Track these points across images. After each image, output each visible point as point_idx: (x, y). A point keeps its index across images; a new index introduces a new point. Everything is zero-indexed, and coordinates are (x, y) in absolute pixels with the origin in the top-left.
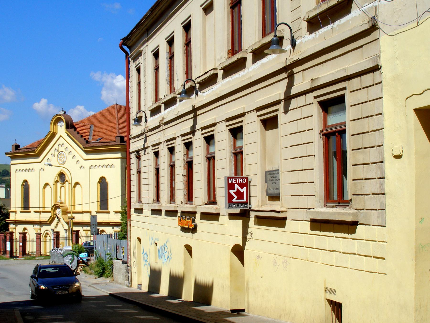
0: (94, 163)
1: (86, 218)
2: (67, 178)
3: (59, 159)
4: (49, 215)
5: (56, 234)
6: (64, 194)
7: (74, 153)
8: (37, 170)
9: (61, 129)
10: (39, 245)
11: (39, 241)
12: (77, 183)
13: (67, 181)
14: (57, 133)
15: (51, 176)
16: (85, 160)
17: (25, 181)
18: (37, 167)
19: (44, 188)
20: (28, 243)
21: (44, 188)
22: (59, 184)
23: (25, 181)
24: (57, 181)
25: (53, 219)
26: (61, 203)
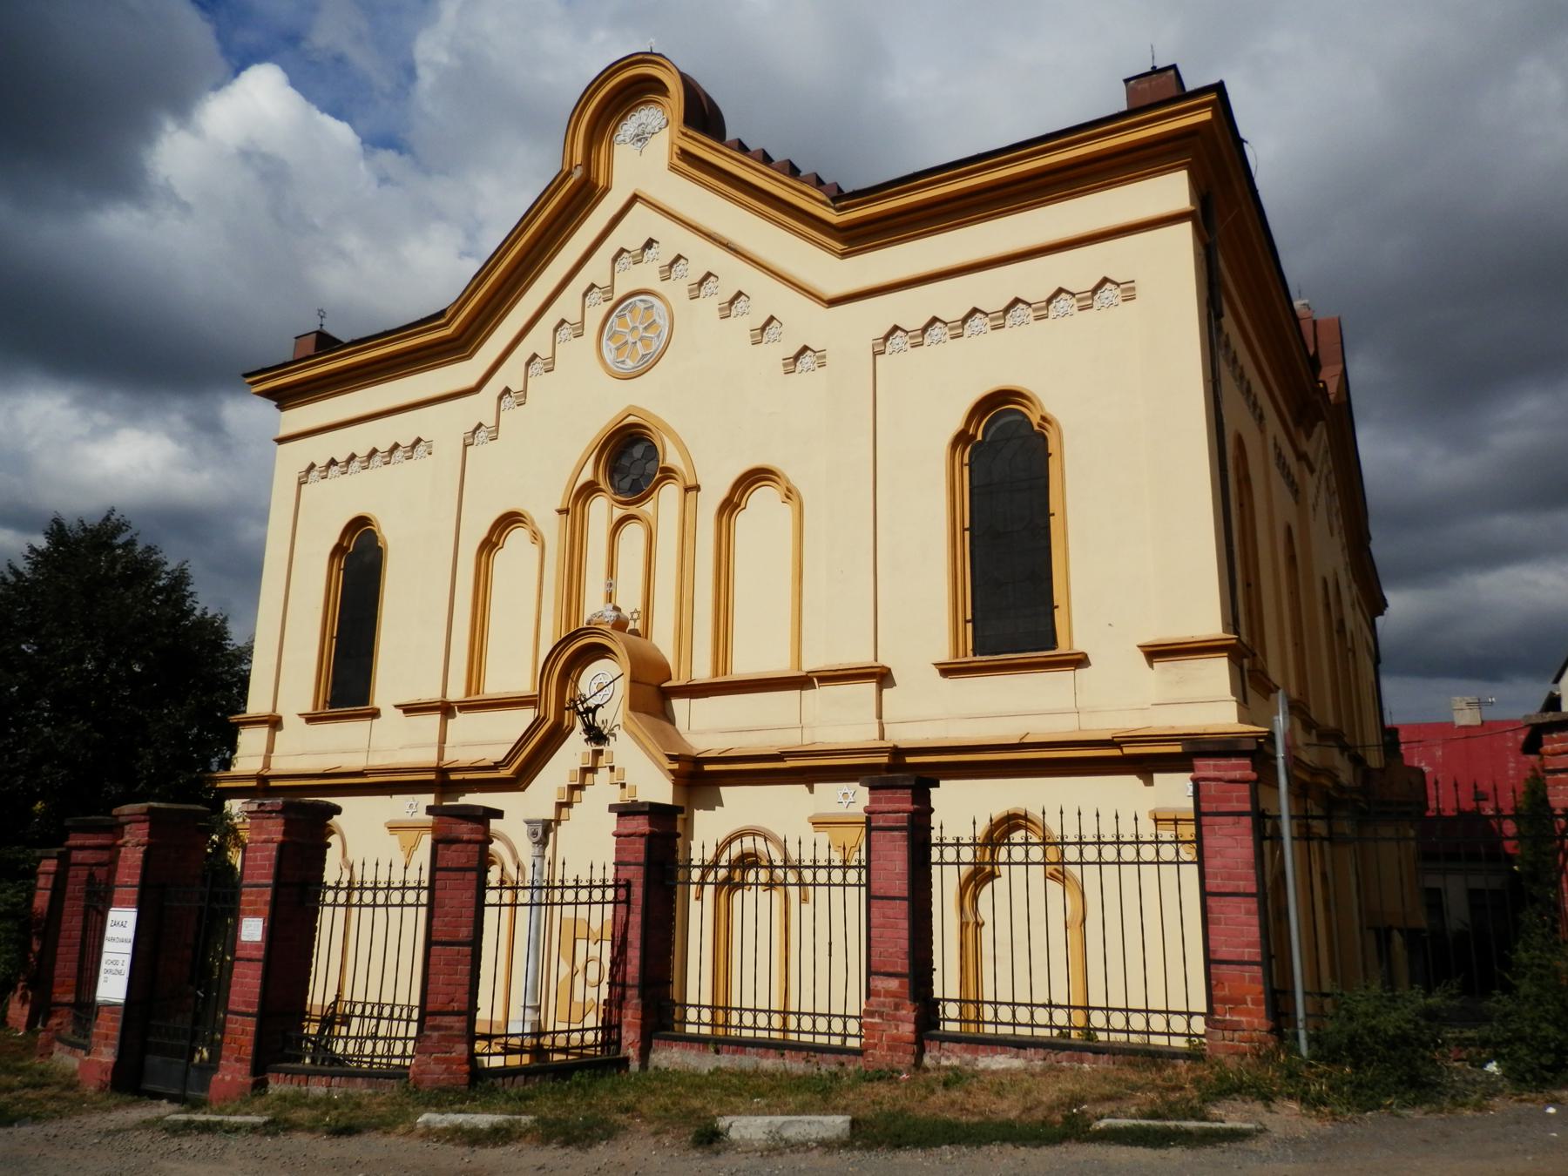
0: (910, 308)
3: (608, 348)
5: (641, 825)
8: (448, 450)
9: (644, 154)
10: (453, 948)
11: (457, 896)
12: (755, 477)
13: (668, 474)
14: (607, 190)
17: (360, 528)
20: (329, 921)
21: (489, 545)
23: (360, 528)
24: (590, 489)
25: (555, 738)
26: (620, 625)
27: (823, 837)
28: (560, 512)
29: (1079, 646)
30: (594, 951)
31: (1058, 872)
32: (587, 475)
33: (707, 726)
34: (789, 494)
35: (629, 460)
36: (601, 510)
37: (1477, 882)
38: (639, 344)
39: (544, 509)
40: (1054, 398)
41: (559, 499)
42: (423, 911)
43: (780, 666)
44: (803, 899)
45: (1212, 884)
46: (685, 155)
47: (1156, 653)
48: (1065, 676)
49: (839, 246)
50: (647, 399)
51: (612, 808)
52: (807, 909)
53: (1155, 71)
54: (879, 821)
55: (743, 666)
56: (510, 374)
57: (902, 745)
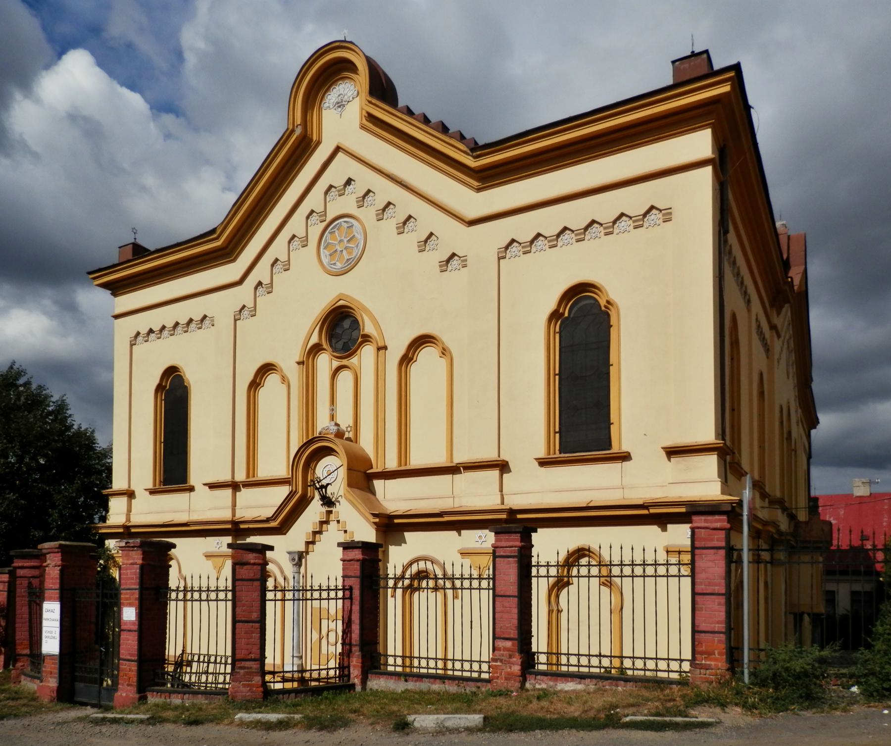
0: (522, 227)
1: (477, 493)
2: (368, 328)
4: (280, 493)
6: (351, 398)
7: (407, 204)
8: (225, 322)
9: (343, 116)
10: (249, 624)
13: (367, 339)
14: (319, 143)
15: (287, 323)
16: (472, 223)
17: (172, 374)
18: (220, 306)
19: (255, 385)
21: (255, 385)
22: (325, 362)
23: (172, 374)
24: (316, 349)
25: (303, 503)
26: (340, 435)
27: (467, 562)
28: (299, 363)
29: (625, 448)
30: (332, 626)
31: (607, 581)
32: (314, 339)
33: (395, 496)
34: (444, 352)
35: (341, 329)
36: (325, 362)
37: (857, 587)
38: (344, 252)
39: (288, 359)
40: (615, 289)
41: (297, 355)
42: (229, 604)
43: (439, 459)
44: (455, 597)
45: (699, 588)
46: (371, 118)
47: (672, 452)
48: (616, 466)
49: (476, 184)
50: (352, 288)
51: (339, 545)
52: (458, 602)
53: (694, 55)
54: (500, 552)
55: (416, 461)
56: (261, 272)
57: (515, 508)
